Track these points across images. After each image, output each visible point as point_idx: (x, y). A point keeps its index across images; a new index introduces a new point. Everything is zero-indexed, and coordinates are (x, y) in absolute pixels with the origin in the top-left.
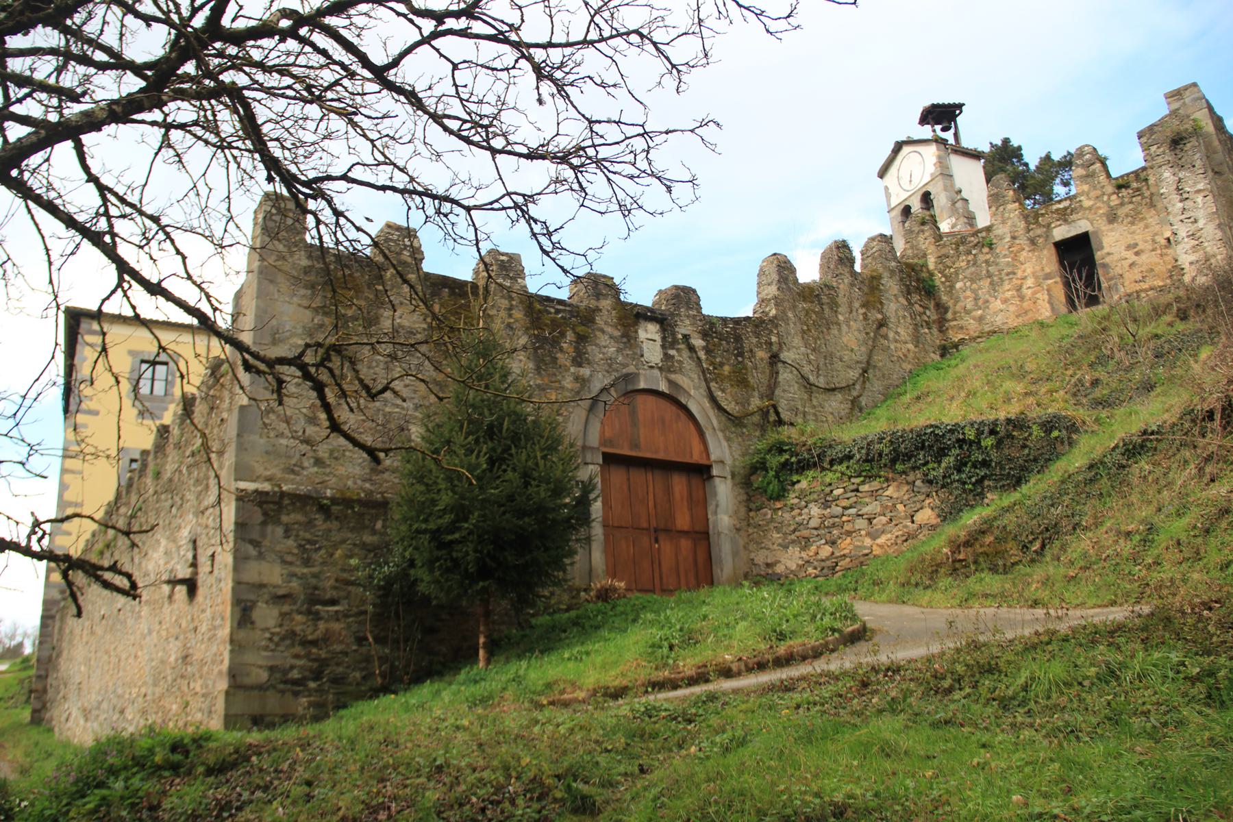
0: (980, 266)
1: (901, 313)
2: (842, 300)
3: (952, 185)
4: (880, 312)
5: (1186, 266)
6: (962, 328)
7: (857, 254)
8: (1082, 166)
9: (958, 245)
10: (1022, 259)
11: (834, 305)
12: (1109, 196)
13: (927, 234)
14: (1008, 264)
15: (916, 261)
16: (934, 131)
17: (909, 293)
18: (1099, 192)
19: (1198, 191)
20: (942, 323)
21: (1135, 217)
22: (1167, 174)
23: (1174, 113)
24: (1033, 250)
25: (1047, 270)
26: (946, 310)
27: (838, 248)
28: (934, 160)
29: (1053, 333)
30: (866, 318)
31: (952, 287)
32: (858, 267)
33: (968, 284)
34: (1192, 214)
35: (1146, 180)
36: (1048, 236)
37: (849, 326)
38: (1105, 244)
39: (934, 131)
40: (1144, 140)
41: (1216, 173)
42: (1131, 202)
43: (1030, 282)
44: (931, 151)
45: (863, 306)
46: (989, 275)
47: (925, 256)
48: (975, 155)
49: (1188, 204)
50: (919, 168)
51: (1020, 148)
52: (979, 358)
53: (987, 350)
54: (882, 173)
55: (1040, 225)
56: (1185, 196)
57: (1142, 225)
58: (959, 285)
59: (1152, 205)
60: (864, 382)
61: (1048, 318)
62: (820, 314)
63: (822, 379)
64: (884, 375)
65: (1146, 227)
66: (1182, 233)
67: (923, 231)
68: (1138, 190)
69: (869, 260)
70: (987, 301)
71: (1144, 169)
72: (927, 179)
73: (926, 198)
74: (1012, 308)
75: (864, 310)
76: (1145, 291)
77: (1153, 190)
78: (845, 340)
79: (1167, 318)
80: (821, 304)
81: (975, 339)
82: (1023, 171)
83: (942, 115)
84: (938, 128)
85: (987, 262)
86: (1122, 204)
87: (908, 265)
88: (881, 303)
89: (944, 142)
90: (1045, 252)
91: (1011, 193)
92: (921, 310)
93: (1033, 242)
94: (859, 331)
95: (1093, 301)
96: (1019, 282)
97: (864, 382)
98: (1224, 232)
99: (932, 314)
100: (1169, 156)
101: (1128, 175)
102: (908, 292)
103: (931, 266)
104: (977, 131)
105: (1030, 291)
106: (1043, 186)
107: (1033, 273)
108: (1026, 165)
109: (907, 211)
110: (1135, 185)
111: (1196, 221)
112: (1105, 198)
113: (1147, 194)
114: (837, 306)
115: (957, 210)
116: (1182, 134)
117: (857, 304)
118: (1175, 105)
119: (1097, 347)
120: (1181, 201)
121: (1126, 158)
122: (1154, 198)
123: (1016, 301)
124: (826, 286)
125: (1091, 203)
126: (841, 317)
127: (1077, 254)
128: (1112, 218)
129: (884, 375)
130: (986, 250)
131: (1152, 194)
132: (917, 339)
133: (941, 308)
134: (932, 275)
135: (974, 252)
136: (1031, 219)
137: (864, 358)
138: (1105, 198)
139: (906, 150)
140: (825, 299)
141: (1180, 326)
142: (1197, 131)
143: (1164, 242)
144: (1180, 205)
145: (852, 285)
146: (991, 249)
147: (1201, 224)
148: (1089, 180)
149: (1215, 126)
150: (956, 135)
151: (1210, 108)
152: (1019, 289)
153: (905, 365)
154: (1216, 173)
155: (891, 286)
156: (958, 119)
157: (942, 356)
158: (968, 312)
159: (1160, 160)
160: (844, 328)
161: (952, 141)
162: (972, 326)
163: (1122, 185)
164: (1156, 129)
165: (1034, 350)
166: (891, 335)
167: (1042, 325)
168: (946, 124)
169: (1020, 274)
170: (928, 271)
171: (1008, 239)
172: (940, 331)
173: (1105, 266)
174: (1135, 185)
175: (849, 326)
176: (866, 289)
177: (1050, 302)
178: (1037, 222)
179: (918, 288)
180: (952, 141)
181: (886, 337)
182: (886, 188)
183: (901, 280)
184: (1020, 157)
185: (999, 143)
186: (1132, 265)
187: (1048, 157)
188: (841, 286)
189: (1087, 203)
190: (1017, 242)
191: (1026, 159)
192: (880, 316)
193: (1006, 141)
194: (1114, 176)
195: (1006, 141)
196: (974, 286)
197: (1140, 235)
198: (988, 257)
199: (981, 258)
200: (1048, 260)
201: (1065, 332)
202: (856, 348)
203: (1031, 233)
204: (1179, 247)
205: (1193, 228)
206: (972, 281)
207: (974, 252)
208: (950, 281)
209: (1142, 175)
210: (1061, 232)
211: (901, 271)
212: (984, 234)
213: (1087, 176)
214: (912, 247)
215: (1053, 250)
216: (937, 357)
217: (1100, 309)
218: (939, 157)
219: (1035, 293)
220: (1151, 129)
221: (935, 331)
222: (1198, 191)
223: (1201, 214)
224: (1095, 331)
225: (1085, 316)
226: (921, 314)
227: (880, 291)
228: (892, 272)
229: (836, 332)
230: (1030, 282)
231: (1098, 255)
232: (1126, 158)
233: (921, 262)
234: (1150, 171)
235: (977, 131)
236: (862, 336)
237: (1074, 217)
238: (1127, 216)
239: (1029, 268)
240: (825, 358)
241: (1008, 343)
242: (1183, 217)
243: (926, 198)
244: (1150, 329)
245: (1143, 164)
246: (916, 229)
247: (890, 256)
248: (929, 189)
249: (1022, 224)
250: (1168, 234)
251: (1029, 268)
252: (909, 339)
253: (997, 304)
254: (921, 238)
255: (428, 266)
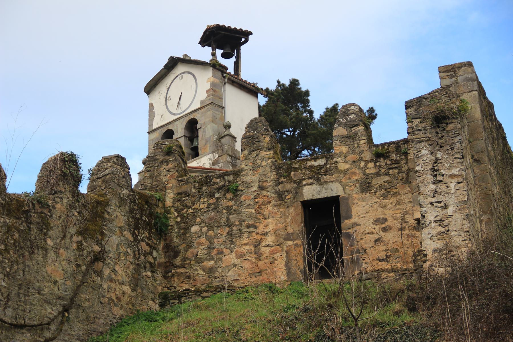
0: (221, 212)
1: (122, 249)
2: (56, 222)
3: (222, 118)
4: (99, 243)
5: (430, 253)
6: (189, 277)
7: (85, 173)
8: (345, 125)
9: (201, 184)
10: (266, 213)
11: (45, 226)
12: (367, 162)
13: (170, 166)
14: (250, 216)
15: (152, 193)
16: (214, 55)
17: (137, 227)
18: (356, 157)
19: (453, 176)
20: (167, 269)
21: (388, 191)
22: (424, 152)
23: (444, 89)
24: (279, 206)
25: (290, 230)
26: (176, 254)
27: (64, 161)
28: (208, 86)
29: (279, 300)
30: (80, 246)
31: (187, 229)
32: (83, 189)
33: (205, 229)
34: (443, 199)
35: (406, 154)
36: (297, 192)
37: (57, 254)
38: (353, 214)
39: (214, 55)
40: (411, 111)
41: (476, 160)
42: (387, 174)
43: (270, 239)
44: (206, 78)
45: (79, 233)
46: (229, 224)
47: (164, 189)
48: (253, 90)
49: (442, 187)
50: (190, 92)
51: (307, 93)
52: (195, 315)
53: (208, 307)
54: (150, 89)
55: (291, 180)
56: (439, 178)
57: (394, 200)
58: (194, 229)
59: (408, 181)
60: (62, 323)
61: (282, 283)
62: (25, 234)
63: (9, 312)
64: (88, 318)
65: (398, 203)
66: (430, 217)
67: (167, 162)
68: (396, 162)
69: (99, 182)
70: (221, 253)
71: (405, 141)
72: (197, 105)
73: (192, 126)
74: (247, 265)
75: (80, 238)
76: (387, 271)
77: (410, 164)
78: (49, 269)
79: (396, 306)
80: (29, 222)
81: (198, 292)
82: (306, 119)
83: (226, 39)
84: (219, 52)
85: (229, 208)
86: (378, 174)
87: (141, 196)
88: (102, 234)
89: (223, 69)
90: (291, 210)
91: (268, 139)
92: (148, 249)
93: (280, 196)
94: (69, 261)
95: (324, 274)
96: (259, 237)
97: (62, 323)
98: (474, 224)
99: (159, 256)
100: (431, 134)
101: (389, 144)
102: (136, 227)
103: (169, 202)
104: (262, 65)
105: (268, 249)
106: (326, 139)
107: (276, 231)
108: (311, 112)
109: (169, 134)
110: (394, 156)
111: (446, 207)
112: (362, 164)
113: (405, 168)
114: (48, 227)
115: (222, 145)
116: (448, 111)
117: (72, 230)
118: (448, 82)
119: (319, 324)
120: (434, 183)
121: (390, 128)
122: (411, 174)
123: (252, 258)
124: (39, 202)
125: (347, 166)
126: (50, 242)
127: (323, 220)
128: (366, 187)
129: (88, 318)
130: (229, 196)
131: (409, 170)
132: (136, 282)
133: (172, 251)
134: (168, 212)
135: (217, 195)
136: (283, 171)
137: (69, 294)
138: (362, 164)
139: (180, 69)
140: (35, 217)
141: (407, 318)
142: (461, 113)
143: (412, 222)
144: (432, 187)
145: (71, 207)
146: (236, 196)
147: (450, 211)
148: (349, 141)
149: (483, 112)
150: (237, 65)
151: (482, 92)
152: (257, 245)
153: (115, 310)
154: (476, 160)
155: (118, 216)
156: (242, 47)
157: (162, 306)
158: (199, 261)
159: (420, 135)
160: (51, 255)
161: (231, 70)
162: (200, 275)
163: (381, 153)
164: (425, 102)
165: (254, 317)
166: (107, 272)
167: (271, 289)
168: (228, 51)
169: (261, 229)
170: (164, 207)
171: (255, 188)
172: (165, 277)
173: (349, 236)
174: (394, 156)
175: (57, 254)
176: (87, 214)
177: (286, 265)
178: (288, 176)
179: (148, 224)
180: (231, 70)
181: (99, 273)
182: (151, 106)
183: (131, 211)
184: (306, 103)
185: (287, 83)
186: (377, 241)
187: (327, 108)
188: (58, 206)
189: (343, 166)
190: (265, 193)
191: (312, 106)
192: (97, 248)
193: (294, 83)
194: (376, 141)
195: (294, 83)
196: (211, 233)
197: (391, 212)
198: (231, 203)
199: (224, 203)
200: (293, 220)
201: (292, 301)
202: (60, 281)
203: (280, 187)
204: (425, 231)
205: (442, 213)
206: (210, 227)
207: (217, 195)
208: (186, 222)
209: (403, 148)
210: (311, 192)
211: (133, 201)
212: (231, 178)
213: (348, 137)
214: (151, 177)
215: (300, 207)
216: (155, 307)
217: (331, 284)
218: (213, 84)
219: (273, 253)
220: (420, 100)
221: (159, 276)
222: (453, 176)
223: (452, 200)
224: (322, 307)
225: (317, 290)
226: (146, 254)
227: (104, 219)
228: (122, 201)
229: (40, 258)
230: (270, 239)
231: (346, 223)
232: (390, 128)
233: (157, 195)
234: (410, 145)
235: (262, 65)
236: (71, 268)
237: (327, 178)
238: (381, 187)
239: (271, 224)
240: (20, 287)
241: (232, 303)
242: (433, 200)
243: (192, 126)
244: (377, 315)
245: (405, 136)
246: (160, 158)
247: (123, 182)
248: (197, 116)
249: (273, 175)
250: (418, 215)
251: (271, 224)
252: (126, 279)
253: (231, 258)
254: (163, 169)
255: (211, 48)
